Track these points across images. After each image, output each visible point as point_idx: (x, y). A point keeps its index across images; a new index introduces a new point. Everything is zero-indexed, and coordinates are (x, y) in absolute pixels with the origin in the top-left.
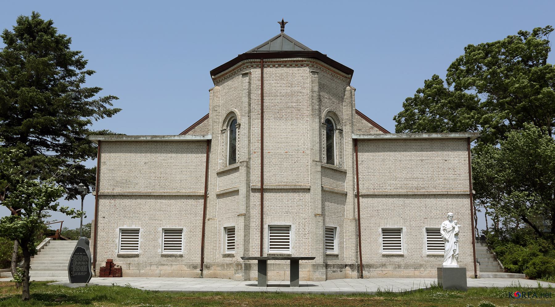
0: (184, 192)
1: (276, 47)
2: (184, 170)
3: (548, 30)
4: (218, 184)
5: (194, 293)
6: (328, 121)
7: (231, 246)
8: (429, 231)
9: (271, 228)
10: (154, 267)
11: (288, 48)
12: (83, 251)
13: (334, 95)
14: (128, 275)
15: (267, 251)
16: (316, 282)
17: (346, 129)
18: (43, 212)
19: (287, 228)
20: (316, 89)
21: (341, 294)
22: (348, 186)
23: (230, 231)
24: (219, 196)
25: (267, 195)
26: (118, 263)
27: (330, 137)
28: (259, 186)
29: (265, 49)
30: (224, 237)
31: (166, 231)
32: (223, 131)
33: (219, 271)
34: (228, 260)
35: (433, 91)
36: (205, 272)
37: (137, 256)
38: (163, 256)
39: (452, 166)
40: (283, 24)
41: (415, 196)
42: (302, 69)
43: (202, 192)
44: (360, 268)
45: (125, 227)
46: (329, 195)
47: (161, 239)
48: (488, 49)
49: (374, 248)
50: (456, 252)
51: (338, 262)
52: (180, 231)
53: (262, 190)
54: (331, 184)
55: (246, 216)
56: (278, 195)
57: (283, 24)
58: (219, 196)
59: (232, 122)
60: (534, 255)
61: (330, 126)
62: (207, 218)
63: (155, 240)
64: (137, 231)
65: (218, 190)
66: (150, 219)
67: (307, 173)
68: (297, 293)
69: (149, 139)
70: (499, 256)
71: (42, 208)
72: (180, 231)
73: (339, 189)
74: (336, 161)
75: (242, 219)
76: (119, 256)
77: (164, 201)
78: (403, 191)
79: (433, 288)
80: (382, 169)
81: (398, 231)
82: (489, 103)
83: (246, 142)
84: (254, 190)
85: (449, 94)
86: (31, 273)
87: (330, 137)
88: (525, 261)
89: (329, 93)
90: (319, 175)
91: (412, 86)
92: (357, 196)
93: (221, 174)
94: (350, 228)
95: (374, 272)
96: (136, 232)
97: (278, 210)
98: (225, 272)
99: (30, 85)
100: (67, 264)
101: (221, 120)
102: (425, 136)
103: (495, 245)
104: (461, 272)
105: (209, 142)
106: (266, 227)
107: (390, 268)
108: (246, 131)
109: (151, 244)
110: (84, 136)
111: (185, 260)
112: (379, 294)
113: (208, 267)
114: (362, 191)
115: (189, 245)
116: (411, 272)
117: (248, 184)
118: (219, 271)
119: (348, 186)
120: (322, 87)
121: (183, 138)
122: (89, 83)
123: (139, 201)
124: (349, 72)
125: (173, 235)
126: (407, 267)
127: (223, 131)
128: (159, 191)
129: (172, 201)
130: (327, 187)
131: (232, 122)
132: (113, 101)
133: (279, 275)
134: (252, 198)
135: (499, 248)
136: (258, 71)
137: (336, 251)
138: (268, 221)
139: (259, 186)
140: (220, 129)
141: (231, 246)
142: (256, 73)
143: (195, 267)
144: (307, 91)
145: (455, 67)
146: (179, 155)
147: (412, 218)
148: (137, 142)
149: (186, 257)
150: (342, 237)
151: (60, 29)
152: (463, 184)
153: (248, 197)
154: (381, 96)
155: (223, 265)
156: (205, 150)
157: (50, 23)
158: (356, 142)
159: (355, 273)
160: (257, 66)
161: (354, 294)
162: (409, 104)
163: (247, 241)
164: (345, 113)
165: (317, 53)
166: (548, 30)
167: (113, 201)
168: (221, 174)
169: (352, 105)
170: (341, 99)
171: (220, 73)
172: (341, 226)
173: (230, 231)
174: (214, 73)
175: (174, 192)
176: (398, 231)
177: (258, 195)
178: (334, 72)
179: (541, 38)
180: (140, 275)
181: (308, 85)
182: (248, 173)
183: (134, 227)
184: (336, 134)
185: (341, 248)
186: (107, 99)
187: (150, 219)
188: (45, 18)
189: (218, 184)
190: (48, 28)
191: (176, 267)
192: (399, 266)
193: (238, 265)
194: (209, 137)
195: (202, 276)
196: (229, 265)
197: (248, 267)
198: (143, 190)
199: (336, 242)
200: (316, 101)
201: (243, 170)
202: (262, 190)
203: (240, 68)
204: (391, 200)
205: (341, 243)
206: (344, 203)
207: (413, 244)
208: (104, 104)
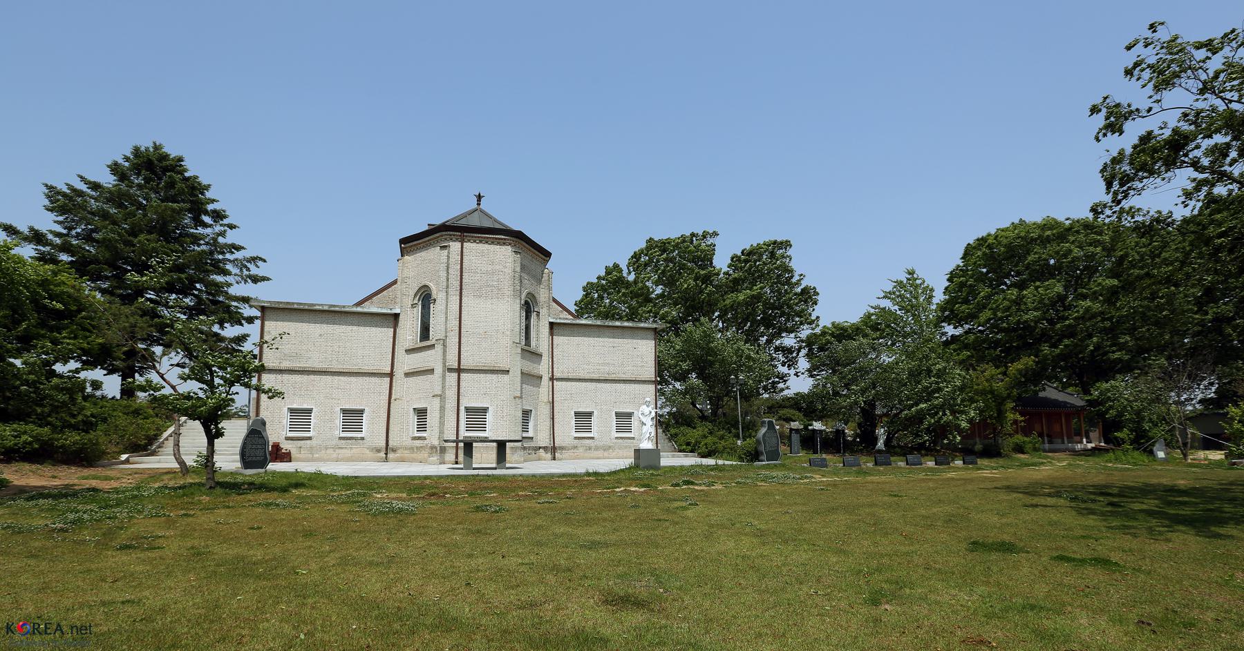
0: (366, 369)
1: (475, 221)
2: (368, 345)
3: (715, 234)
4: (406, 362)
5: (534, 476)
6: (526, 303)
7: (422, 427)
8: (618, 415)
9: (468, 410)
10: (330, 451)
11: (487, 224)
12: (259, 433)
13: (534, 277)
14: (298, 460)
15: (464, 434)
16: (523, 465)
17: (543, 312)
18: (234, 389)
19: (485, 410)
20: (518, 269)
21: (552, 475)
22: (543, 368)
23: (421, 413)
24: (407, 375)
25: (463, 375)
26: (286, 446)
27: (528, 318)
28: (456, 366)
29: (463, 223)
30: (414, 419)
31: (345, 411)
32: (413, 306)
33: (407, 454)
34: (418, 443)
35: (613, 281)
36: (391, 455)
37: (310, 438)
38: (341, 438)
39: (639, 354)
40: (479, 197)
41: (606, 381)
42: (504, 247)
43: (388, 370)
44: (553, 450)
45: (295, 406)
46: (530, 378)
47: (339, 420)
48: (664, 246)
49: (567, 431)
50: (645, 434)
51: (532, 444)
52: (361, 412)
53: (459, 370)
54: (530, 367)
55: (442, 397)
56: (476, 376)
57: (479, 197)
58: (407, 375)
59: (425, 298)
60: (705, 437)
61: (529, 308)
62: (393, 397)
63: (332, 421)
64: (309, 411)
65: (406, 369)
66: (326, 397)
67: (504, 351)
68: (508, 476)
69: (326, 308)
70: (673, 438)
71: (232, 384)
72: (361, 412)
73: (535, 372)
74: (533, 343)
75: (437, 400)
76: (287, 439)
77: (342, 378)
78: (595, 376)
79: (630, 468)
80: (584, 353)
81: (590, 414)
82: (662, 296)
83: (443, 319)
84: (450, 370)
85: (628, 285)
86: (216, 458)
87: (528, 318)
88: (697, 443)
89: (528, 274)
90: (519, 357)
91: (594, 273)
92: (552, 379)
93: (409, 351)
94: (544, 411)
95: (566, 454)
96: (309, 411)
97: (476, 391)
98: (414, 455)
99: (150, 233)
100: (238, 450)
101: (412, 293)
102: (618, 323)
103: (673, 425)
104: (655, 453)
105: (396, 316)
106: (462, 409)
107: (581, 450)
108: (443, 307)
109: (325, 425)
110: (221, 299)
111: (368, 442)
112: (588, 474)
113: (394, 451)
114: (557, 375)
115: (372, 428)
116: (600, 453)
117: (444, 364)
118: (407, 454)
119: (543, 368)
120: (523, 267)
121: (355, 309)
122: (231, 238)
123: (312, 377)
124: (547, 254)
125: (352, 417)
126: (597, 448)
127: (413, 306)
128: (336, 367)
129: (353, 379)
130: (526, 369)
131: (425, 298)
132: (260, 263)
133: (484, 458)
134: (448, 379)
135: (673, 431)
136: (458, 245)
137: (530, 434)
138: (465, 403)
139: (456, 366)
140: (410, 303)
141: (422, 427)
142: (455, 246)
143: (379, 451)
144: (509, 271)
145: (636, 256)
146: (362, 329)
147: (603, 403)
148: (341, 312)
149: (367, 439)
150: (536, 420)
151: (193, 168)
152: (649, 372)
153: (444, 377)
154: (567, 283)
155: (412, 448)
156: (391, 324)
157: (180, 159)
158: (552, 324)
159: (549, 456)
160: (457, 240)
161: (564, 475)
162: (588, 289)
163: (442, 423)
164: (542, 296)
165: (520, 232)
166: (715, 234)
167: (279, 376)
168: (409, 351)
169: (550, 289)
170: (539, 281)
171: (410, 244)
172: (536, 409)
173: (421, 413)
174: (403, 241)
175: (355, 369)
176: (590, 414)
177: (455, 375)
178: (534, 253)
179: (710, 241)
180: (313, 460)
181: (510, 265)
182: (445, 352)
183: (305, 406)
184: (534, 315)
185: (536, 430)
186: (254, 260)
187: (326, 397)
188: (172, 150)
189: (406, 362)
190: (176, 165)
191: (356, 450)
192: (590, 449)
193: (433, 448)
194: (397, 311)
195: (386, 460)
196: (419, 448)
197: (443, 450)
198: (318, 366)
199: (531, 425)
200: (517, 282)
201: (439, 348)
202: (459, 370)
203: (437, 241)
204: (584, 384)
205: (536, 426)
206: (539, 386)
207: (603, 427)
208: (248, 265)
